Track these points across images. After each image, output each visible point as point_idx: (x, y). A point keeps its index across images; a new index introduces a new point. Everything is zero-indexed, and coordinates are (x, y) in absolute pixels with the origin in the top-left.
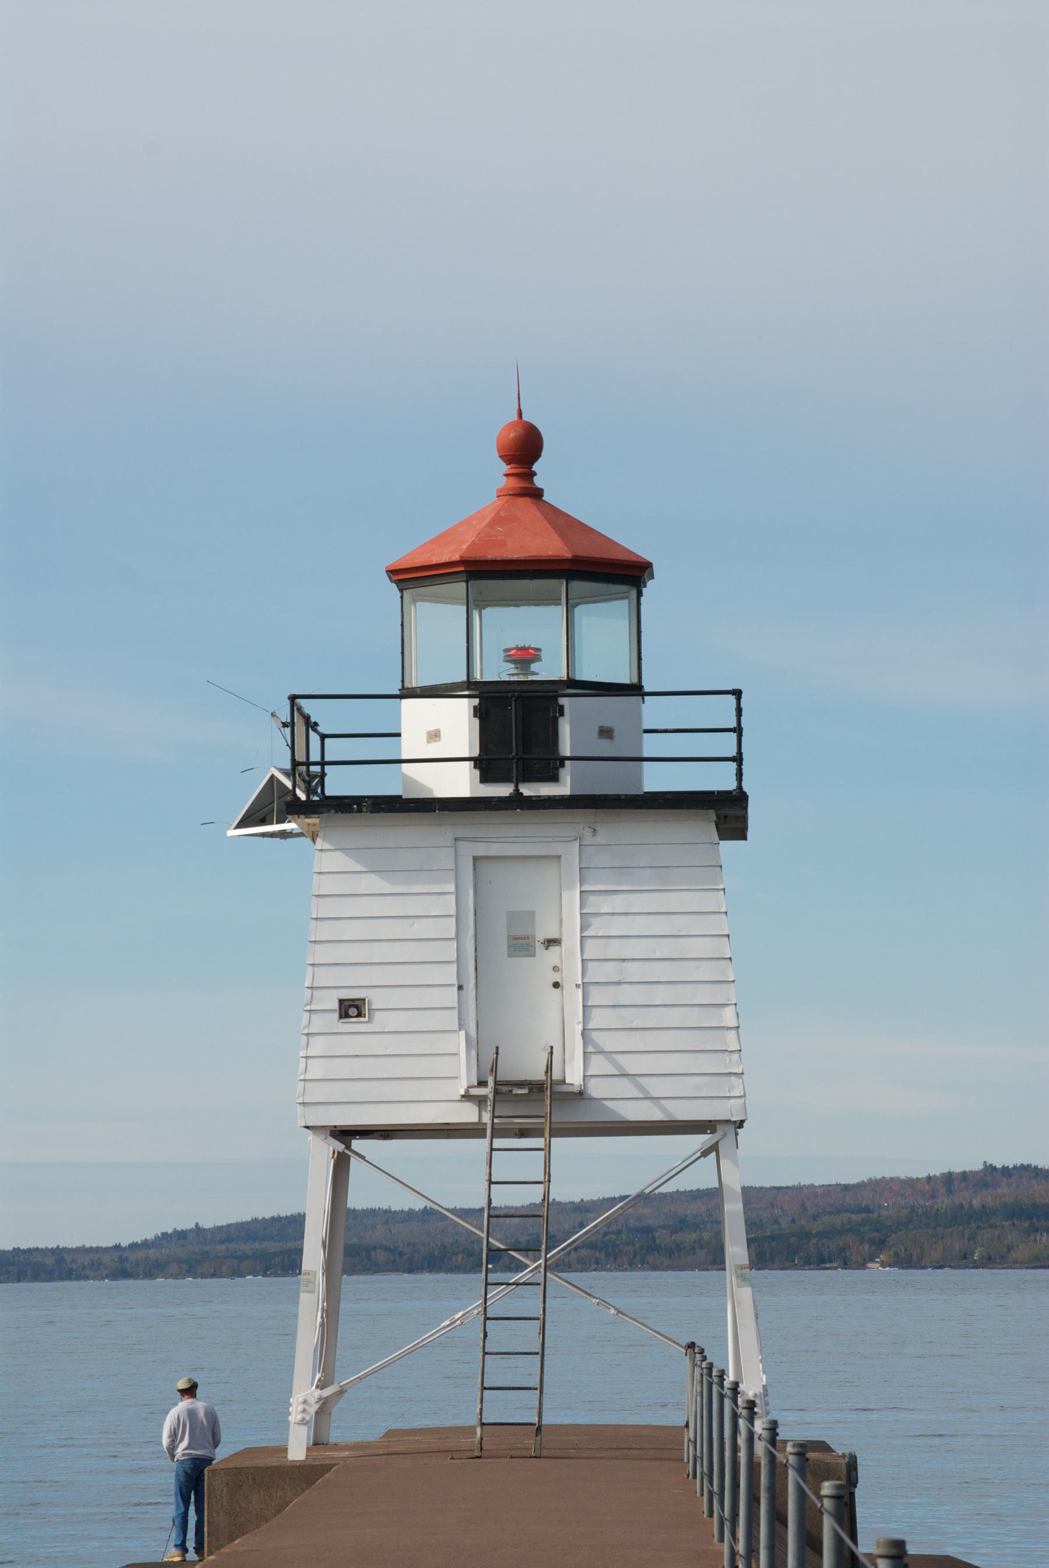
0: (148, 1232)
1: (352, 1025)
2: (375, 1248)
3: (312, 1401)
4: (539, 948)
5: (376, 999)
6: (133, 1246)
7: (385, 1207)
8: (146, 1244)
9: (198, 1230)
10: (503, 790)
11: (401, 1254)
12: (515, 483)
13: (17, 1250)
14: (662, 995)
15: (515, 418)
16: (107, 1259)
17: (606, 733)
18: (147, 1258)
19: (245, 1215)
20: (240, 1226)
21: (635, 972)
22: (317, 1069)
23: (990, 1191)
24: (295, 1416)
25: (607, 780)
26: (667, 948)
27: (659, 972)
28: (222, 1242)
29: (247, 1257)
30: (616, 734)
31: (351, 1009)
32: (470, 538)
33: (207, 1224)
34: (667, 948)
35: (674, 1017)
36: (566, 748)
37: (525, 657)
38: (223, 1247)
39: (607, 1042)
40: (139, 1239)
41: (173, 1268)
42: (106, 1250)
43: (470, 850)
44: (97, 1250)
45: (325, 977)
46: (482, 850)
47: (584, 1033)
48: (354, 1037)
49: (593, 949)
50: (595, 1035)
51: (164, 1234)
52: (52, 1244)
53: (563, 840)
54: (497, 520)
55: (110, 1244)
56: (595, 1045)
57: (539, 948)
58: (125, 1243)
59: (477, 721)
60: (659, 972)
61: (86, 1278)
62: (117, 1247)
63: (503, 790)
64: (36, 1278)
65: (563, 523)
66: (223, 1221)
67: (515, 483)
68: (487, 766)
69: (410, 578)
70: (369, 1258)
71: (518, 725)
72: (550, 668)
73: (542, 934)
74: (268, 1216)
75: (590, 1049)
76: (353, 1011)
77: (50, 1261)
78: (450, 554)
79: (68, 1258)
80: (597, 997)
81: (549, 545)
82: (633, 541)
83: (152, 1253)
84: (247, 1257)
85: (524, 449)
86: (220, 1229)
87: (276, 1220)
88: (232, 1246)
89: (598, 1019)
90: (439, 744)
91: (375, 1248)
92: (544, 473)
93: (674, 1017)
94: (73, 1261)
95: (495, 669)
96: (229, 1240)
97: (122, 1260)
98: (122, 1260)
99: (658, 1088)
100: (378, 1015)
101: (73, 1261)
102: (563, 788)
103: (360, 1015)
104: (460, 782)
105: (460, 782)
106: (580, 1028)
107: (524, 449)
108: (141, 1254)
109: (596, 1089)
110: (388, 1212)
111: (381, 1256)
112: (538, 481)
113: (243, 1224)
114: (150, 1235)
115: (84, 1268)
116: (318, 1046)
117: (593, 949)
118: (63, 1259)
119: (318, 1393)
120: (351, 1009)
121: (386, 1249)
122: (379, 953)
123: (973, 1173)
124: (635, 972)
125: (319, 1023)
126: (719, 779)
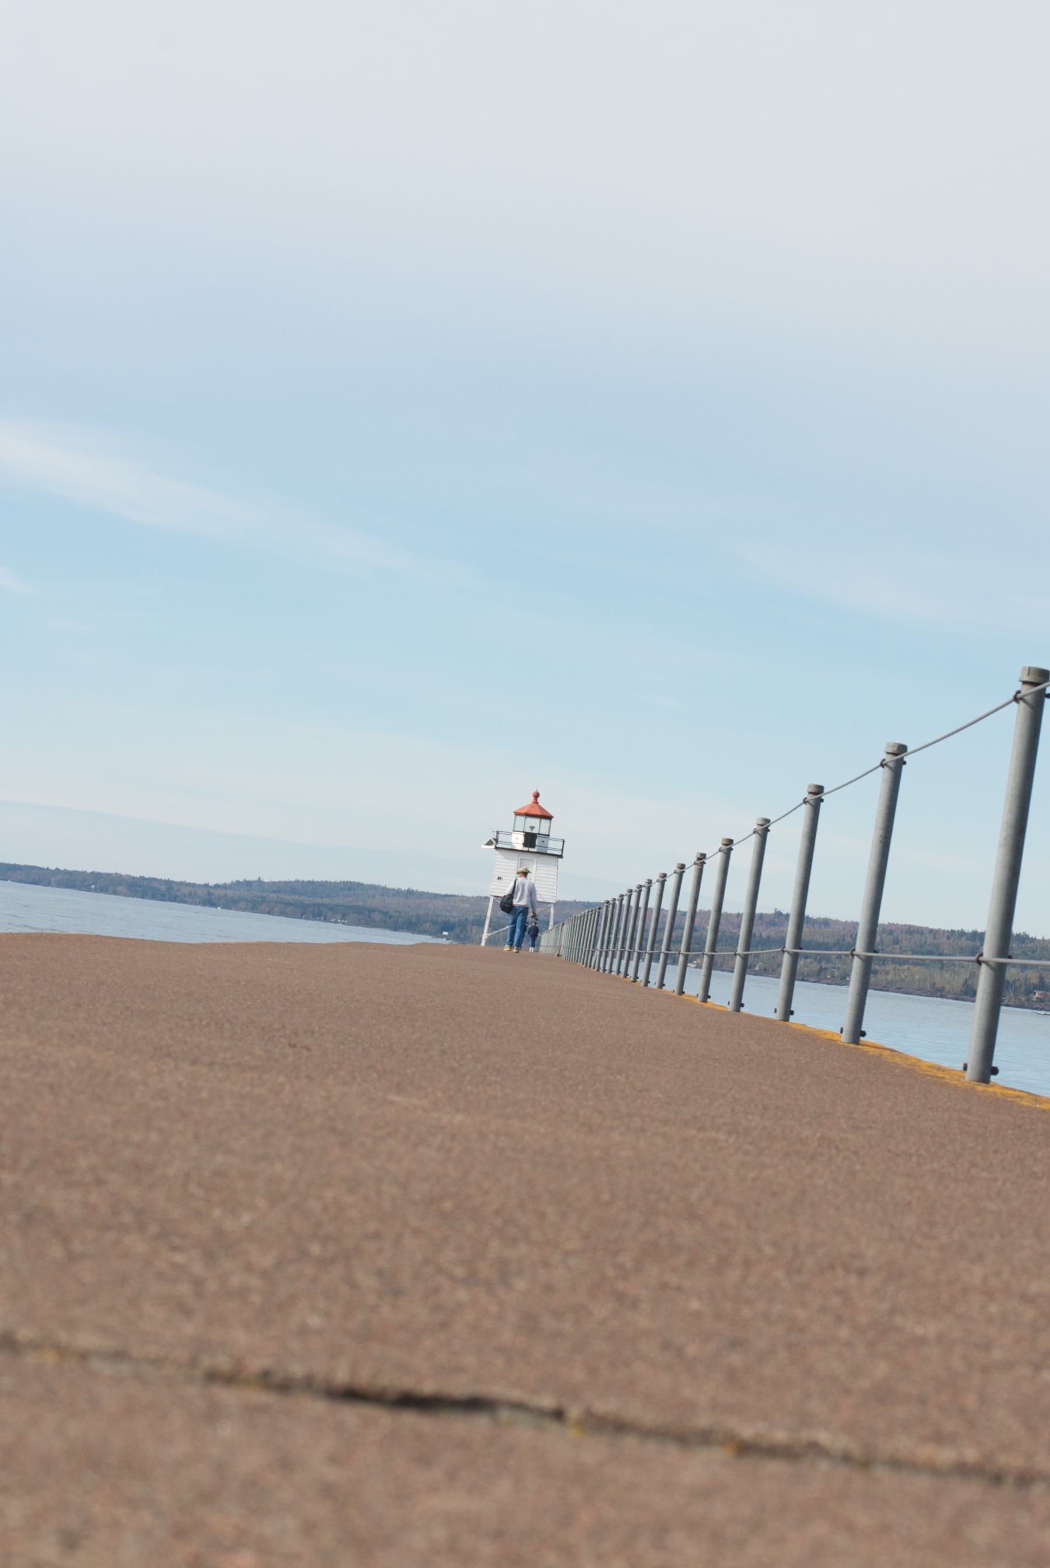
0: (227, 879)
2: (374, 911)
6: (217, 886)
7: (383, 885)
8: (225, 886)
10: (526, 849)
11: (391, 917)
13: (142, 878)
16: (200, 893)
18: (226, 896)
19: (291, 877)
20: (287, 884)
23: (776, 928)
25: (542, 850)
28: (274, 892)
29: (291, 905)
31: (499, 878)
33: (266, 879)
37: (532, 828)
38: (275, 895)
40: (220, 882)
41: (242, 904)
42: (200, 886)
44: (194, 885)
51: (238, 882)
52: (165, 877)
53: (534, 857)
54: (531, 806)
55: (202, 882)
58: (212, 884)
61: (186, 902)
62: (207, 885)
63: (526, 849)
64: (154, 897)
65: (541, 808)
66: (276, 879)
68: (525, 845)
69: (517, 814)
70: (369, 916)
71: (530, 839)
72: (535, 831)
74: (306, 879)
77: (163, 888)
79: (175, 888)
81: (539, 813)
82: (551, 812)
83: (230, 893)
84: (291, 905)
85: (537, 796)
86: (274, 883)
87: (311, 883)
88: (282, 896)
90: (518, 841)
91: (374, 911)
94: (178, 890)
95: (528, 830)
96: (279, 892)
97: (209, 894)
98: (209, 894)
101: (178, 890)
105: (520, 847)
107: (537, 796)
108: (222, 892)
110: (384, 888)
111: (377, 917)
113: (289, 882)
114: (228, 881)
115: (185, 896)
118: (172, 888)
120: (499, 878)
121: (381, 912)
123: (768, 915)
126: (560, 853)
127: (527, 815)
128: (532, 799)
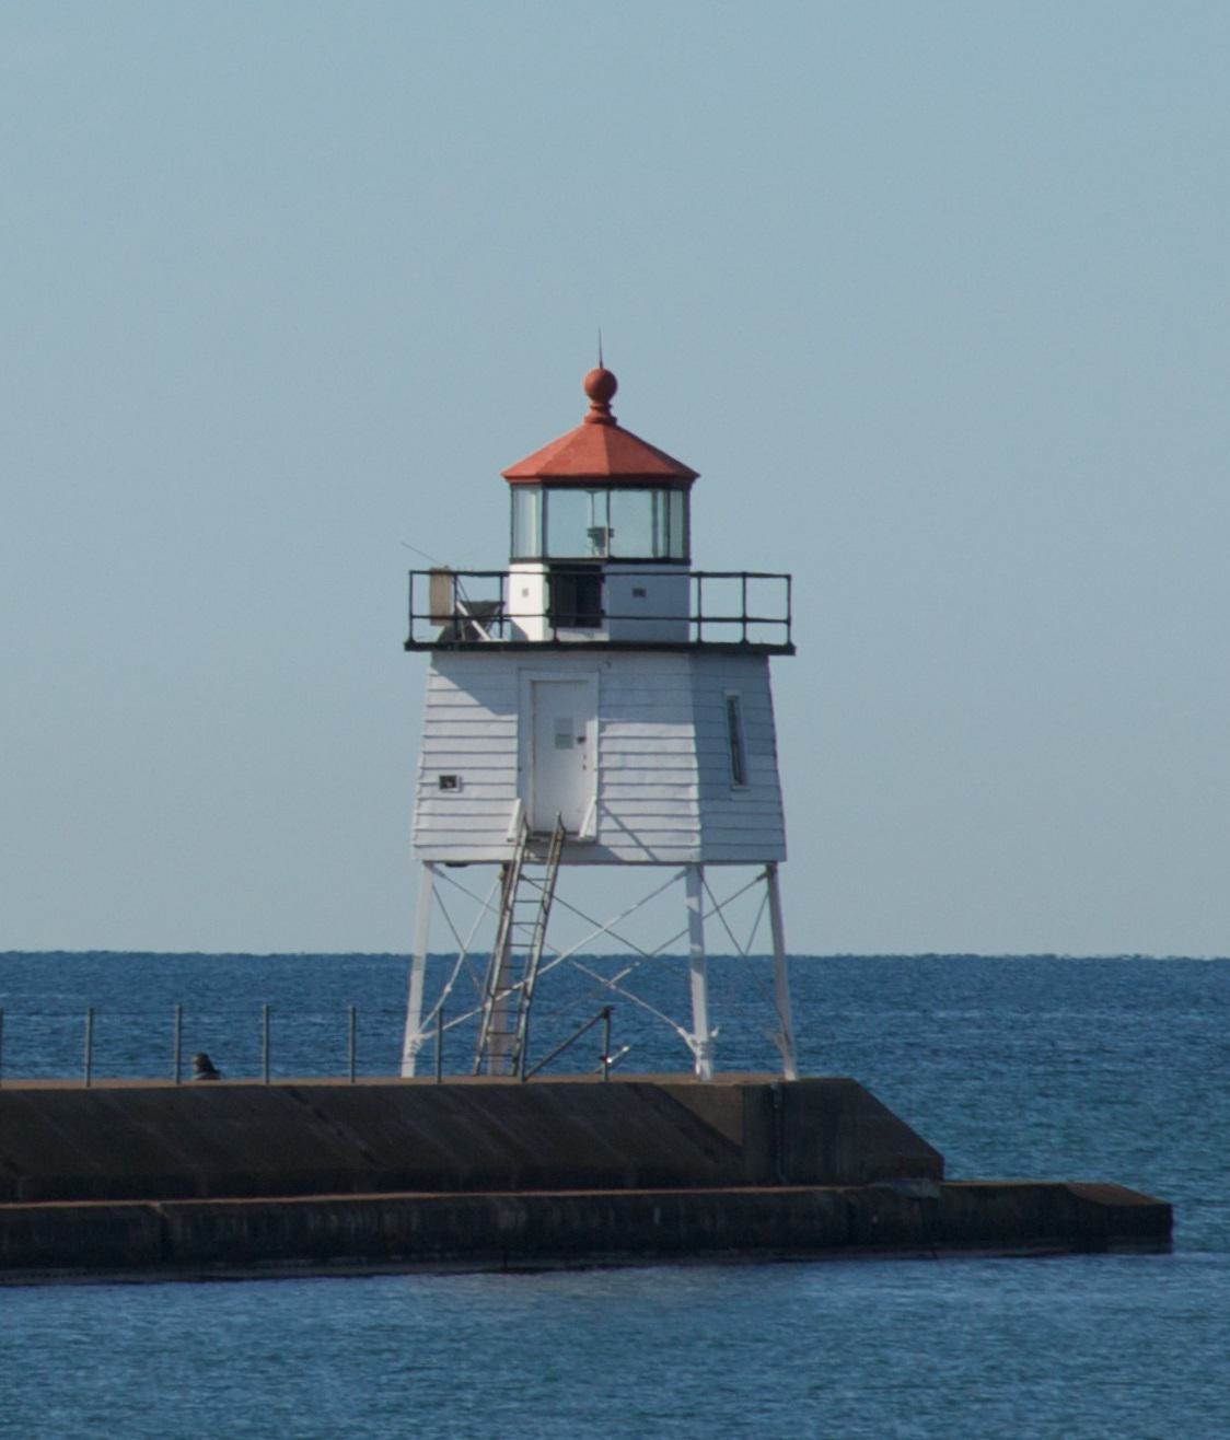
1: (452, 793)
3: (418, 1041)
4: (575, 742)
5: (466, 776)
9: (1050, 958)
12: (595, 414)
14: (650, 777)
15: (598, 367)
17: (639, 593)
21: (632, 761)
22: (425, 823)
24: (407, 1050)
26: (653, 746)
27: (650, 762)
30: (648, 593)
31: (448, 782)
32: (549, 457)
34: (653, 746)
35: (657, 792)
36: (607, 603)
39: (614, 808)
43: (528, 676)
45: (432, 762)
46: (535, 676)
47: (599, 803)
48: (450, 803)
49: (606, 746)
50: (607, 804)
56: (604, 808)
57: (575, 742)
59: (547, 585)
60: (650, 762)
67: (595, 414)
69: (517, 482)
71: (574, 589)
73: (577, 734)
75: (602, 812)
76: (449, 784)
78: (532, 471)
80: (608, 777)
85: (603, 388)
89: (609, 793)
90: (527, 602)
92: (619, 407)
93: (657, 792)
99: (646, 839)
100: (467, 788)
102: (602, 636)
103: (454, 785)
104: (536, 630)
106: (594, 798)
107: (603, 388)
109: (605, 840)
112: (614, 412)
116: (426, 807)
117: (606, 746)
119: (422, 1036)
120: (448, 782)
122: (466, 745)
124: (632, 761)
125: (426, 792)
127: (549, 482)
128: (586, 406)
